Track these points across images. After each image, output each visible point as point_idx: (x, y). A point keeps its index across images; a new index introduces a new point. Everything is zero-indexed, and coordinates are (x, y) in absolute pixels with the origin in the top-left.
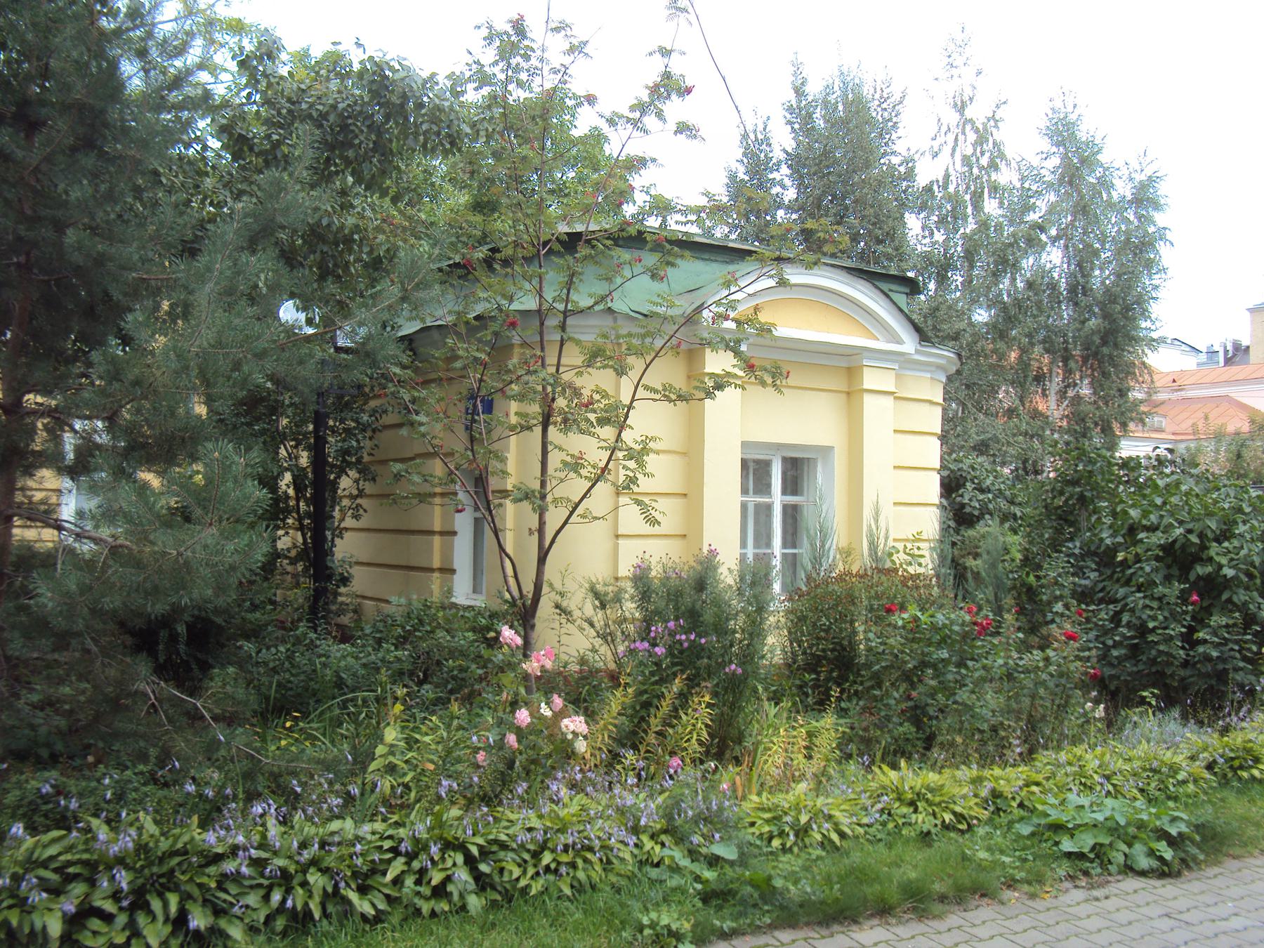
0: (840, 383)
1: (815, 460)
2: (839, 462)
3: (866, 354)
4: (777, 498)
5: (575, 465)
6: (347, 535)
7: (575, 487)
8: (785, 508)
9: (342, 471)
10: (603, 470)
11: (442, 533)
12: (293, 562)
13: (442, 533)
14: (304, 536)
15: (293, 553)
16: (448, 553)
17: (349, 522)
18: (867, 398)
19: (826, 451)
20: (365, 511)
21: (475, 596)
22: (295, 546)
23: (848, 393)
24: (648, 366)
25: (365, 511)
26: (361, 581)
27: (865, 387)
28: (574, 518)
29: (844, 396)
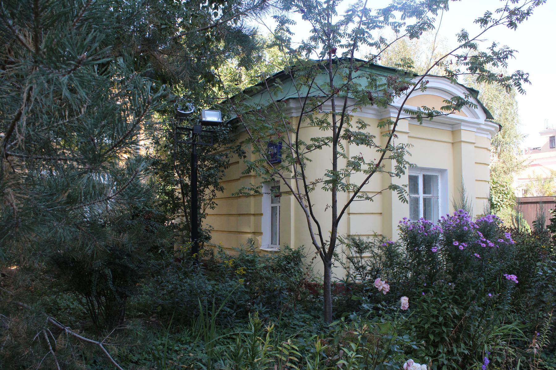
0: (448, 138)
1: (437, 177)
2: (450, 175)
3: (463, 123)
4: (421, 195)
5: (355, 165)
6: (207, 217)
7: (357, 178)
8: (425, 200)
9: (206, 186)
10: (378, 165)
11: (254, 215)
12: (181, 230)
13: (254, 215)
14: (187, 218)
15: (182, 226)
16: (258, 224)
17: (208, 211)
18: (463, 144)
19: (443, 171)
20: (217, 205)
21: (272, 246)
22: (182, 223)
23: (453, 143)
24: (408, 97)
25: (217, 205)
26: (216, 239)
27: (463, 139)
28: (355, 199)
29: (450, 145)
